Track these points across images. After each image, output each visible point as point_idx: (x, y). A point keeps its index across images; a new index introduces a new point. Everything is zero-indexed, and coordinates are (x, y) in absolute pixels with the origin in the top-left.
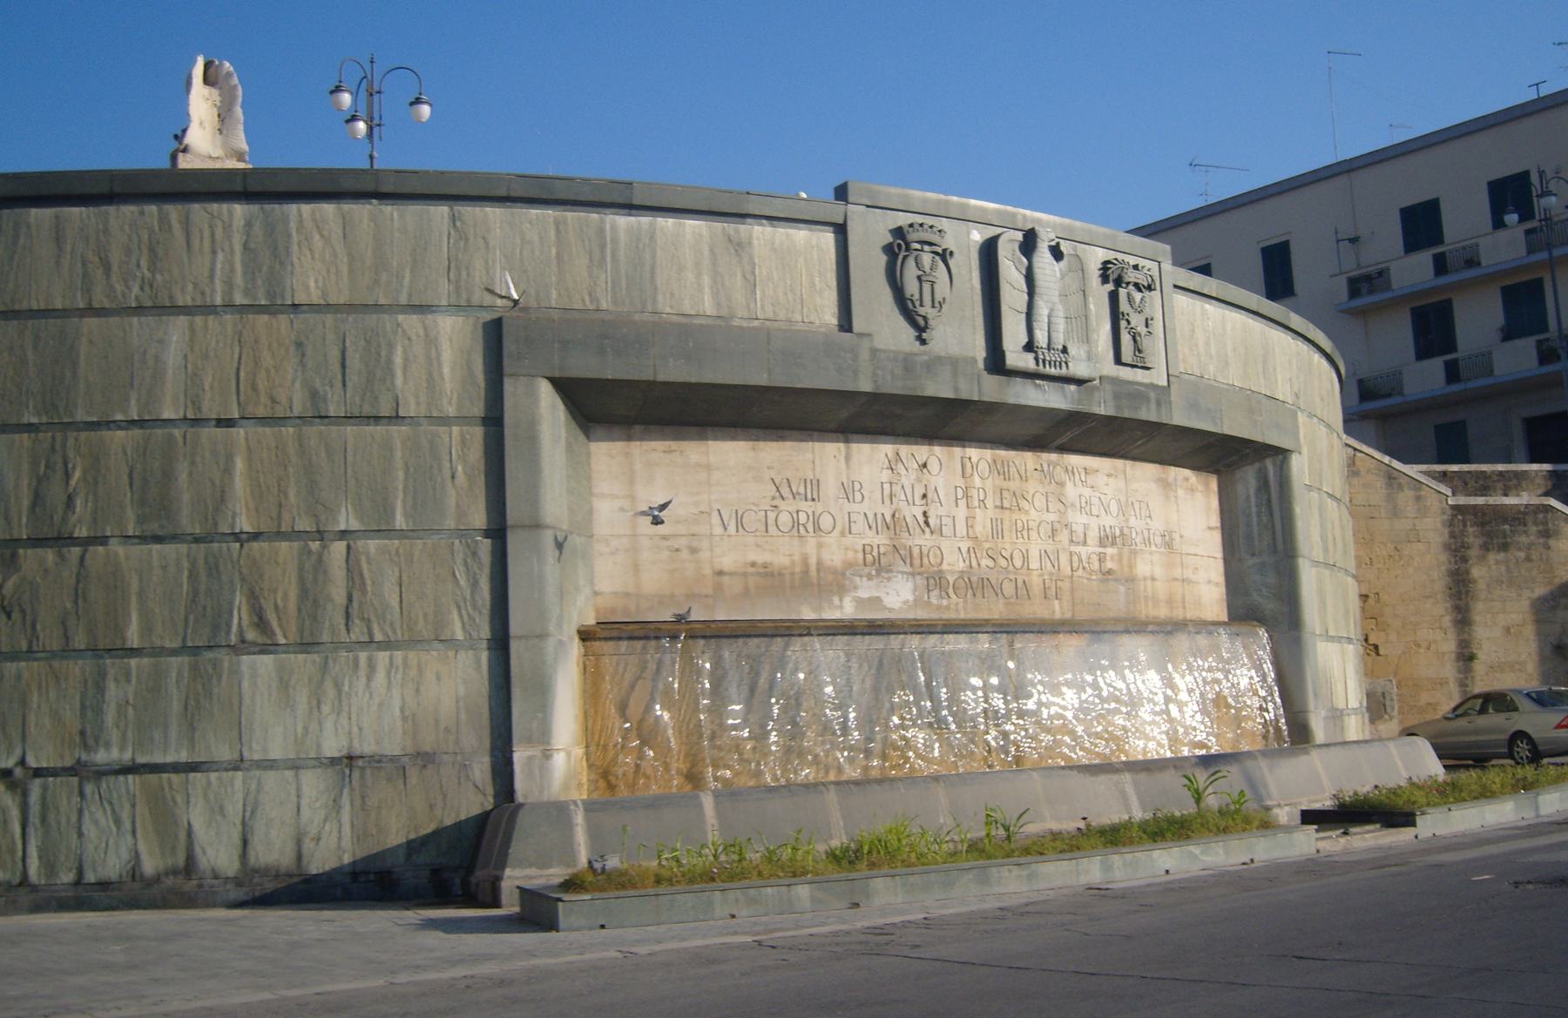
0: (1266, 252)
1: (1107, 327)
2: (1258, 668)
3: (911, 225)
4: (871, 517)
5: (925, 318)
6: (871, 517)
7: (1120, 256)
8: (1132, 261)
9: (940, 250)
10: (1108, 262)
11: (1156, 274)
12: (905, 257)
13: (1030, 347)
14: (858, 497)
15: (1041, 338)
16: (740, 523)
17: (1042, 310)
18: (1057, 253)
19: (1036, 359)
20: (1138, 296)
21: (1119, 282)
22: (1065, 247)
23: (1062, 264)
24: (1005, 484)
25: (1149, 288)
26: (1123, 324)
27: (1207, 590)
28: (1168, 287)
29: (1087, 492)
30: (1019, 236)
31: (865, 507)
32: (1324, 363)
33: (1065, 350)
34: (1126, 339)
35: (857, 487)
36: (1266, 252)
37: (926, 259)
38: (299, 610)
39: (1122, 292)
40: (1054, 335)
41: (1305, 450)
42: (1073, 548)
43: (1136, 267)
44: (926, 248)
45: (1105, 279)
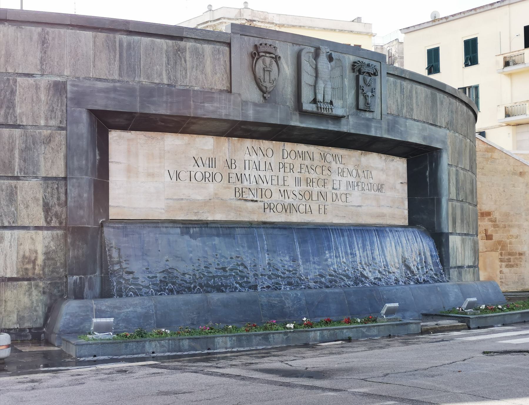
0: (467, 43)
1: (353, 92)
2: (87, 159)
3: (261, 44)
4: (239, 176)
5: (266, 87)
6: (239, 176)
7: (361, 60)
8: (367, 62)
9: (274, 56)
10: (355, 62)
11: (378, 68)
12: (257, 59)
13: (315, 101)
14: (234, 166)
15: (320, 97)
16: (178, 176)
17: (321, 85)
18: (330, 59)
19: (317, 107)
20: (368, 79)
21: (360, 71)
22: (334, 55)
23: (333, 63)
24: (303, 162)
25: (375, 74)
26: (360, 91)
27: (400, 213)
28: (384, 73)
29: (341, 166)
30: (313, 50)
31: (237, 171)
32: (465, 108)
33: (331, 103)
34: (361, 98)
35: (233, 162)
36: (467, 43)
37: (268, 60)
38: (437, 116)
39: (361, 77)
40: (326, 96)
41: (450, 149)
42: (334, 191)
43: (368, 65)
44: (267, 55)
45: (353, 70)
